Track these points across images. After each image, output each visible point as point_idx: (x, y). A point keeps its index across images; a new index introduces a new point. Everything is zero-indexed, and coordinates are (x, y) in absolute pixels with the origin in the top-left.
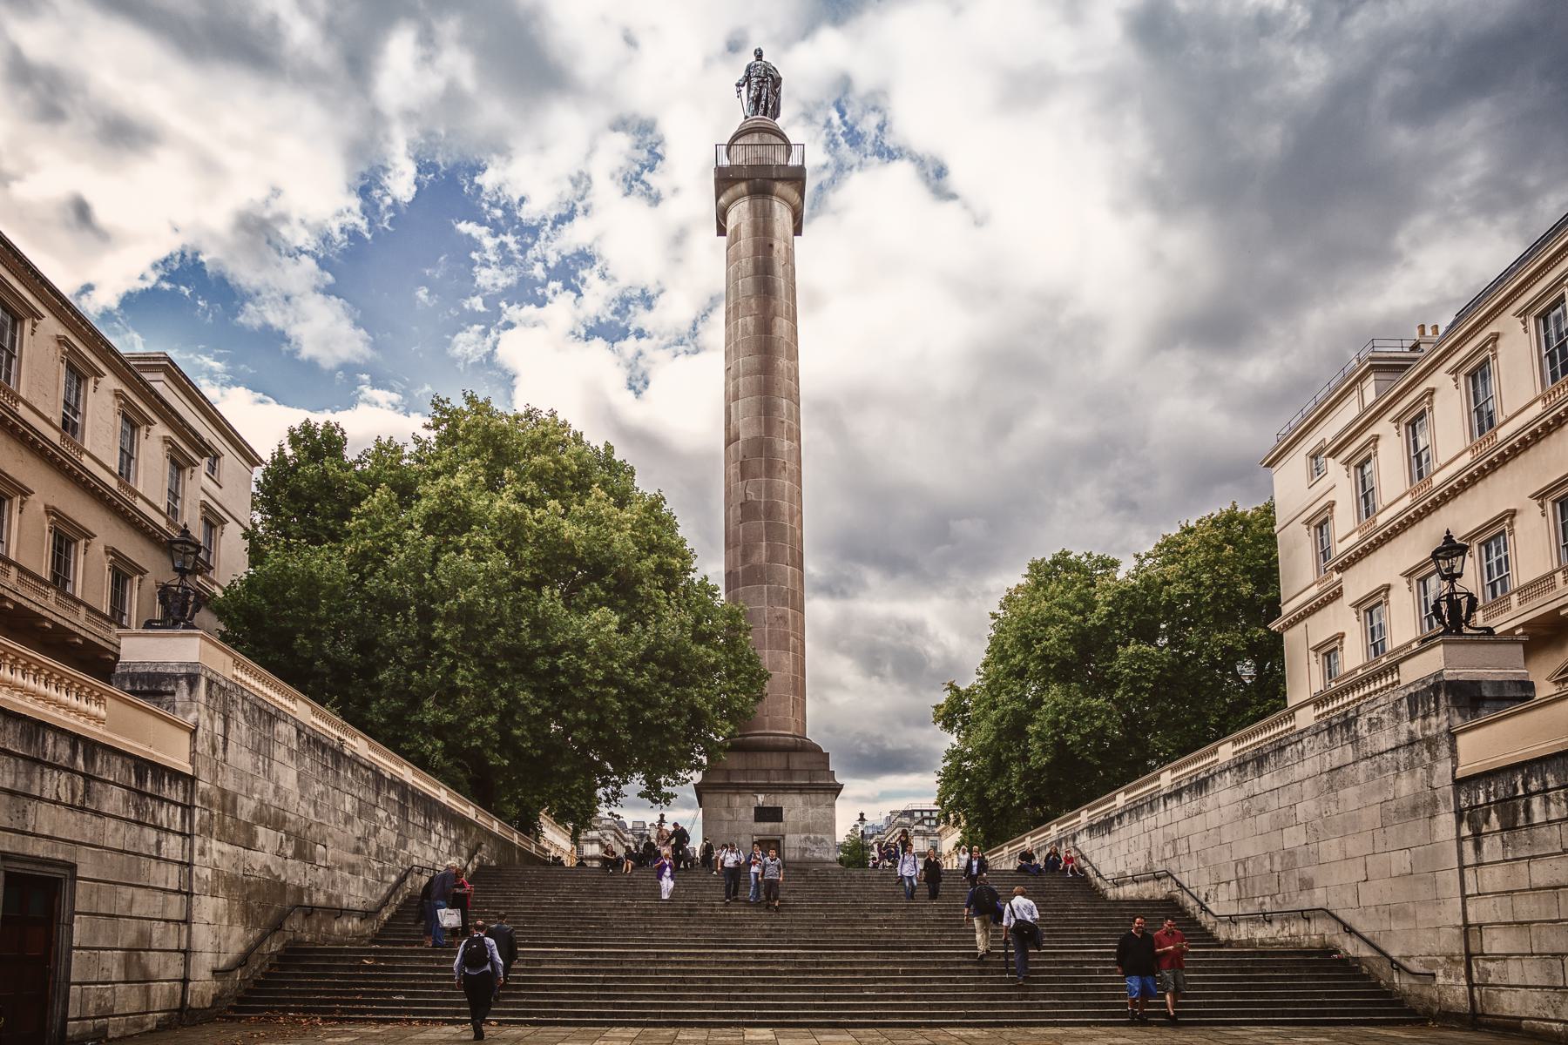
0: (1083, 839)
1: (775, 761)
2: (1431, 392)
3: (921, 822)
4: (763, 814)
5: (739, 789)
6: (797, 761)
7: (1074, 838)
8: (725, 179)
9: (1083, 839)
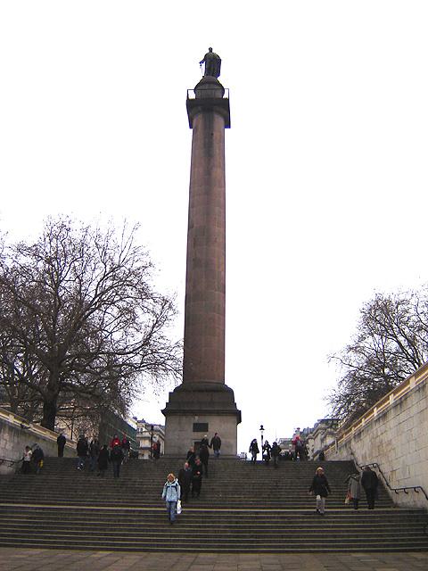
3: (331, 427)
4: (201, 427)
5: (185, 413)
8: (190, 104)
9: (353, 443)
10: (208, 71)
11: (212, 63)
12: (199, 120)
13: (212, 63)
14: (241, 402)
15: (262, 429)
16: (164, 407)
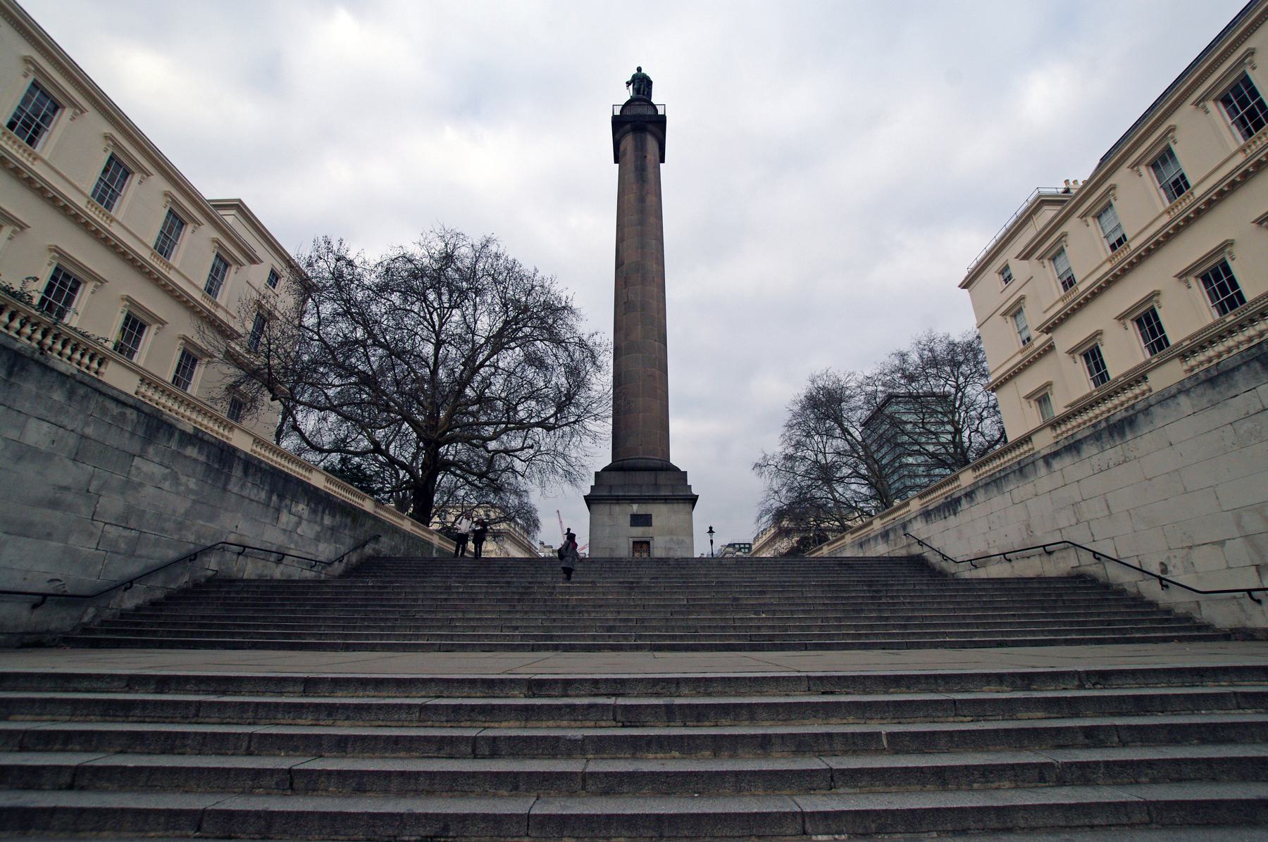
0: (919, 529)
1: (647, 478)
2: (1251, 52)
3: (740, 550)
4: (642, 520)
5: (618, 500)
6: (663, 477)
7: (904, 526)
8: (618, 123)
10: (637, 91)
11: (641, 84)
12: (628, 142)
13: (641, 84)
15: (711, 531)
16: (588, 492)
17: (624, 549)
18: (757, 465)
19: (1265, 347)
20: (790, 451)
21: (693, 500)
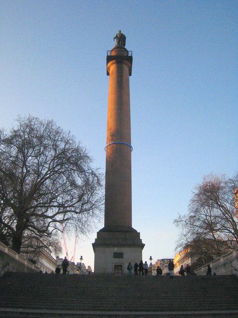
4: (119, 255)
7: (231, 262)
14: (144, 238)
16: (94, 241)
17: (110, 269)
18: (176, 221)
19: (236, 264)
20: (192, 214)
21: (143, 246)
